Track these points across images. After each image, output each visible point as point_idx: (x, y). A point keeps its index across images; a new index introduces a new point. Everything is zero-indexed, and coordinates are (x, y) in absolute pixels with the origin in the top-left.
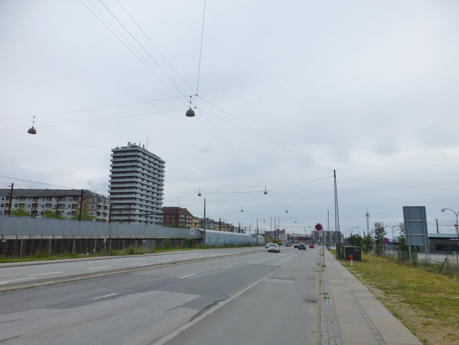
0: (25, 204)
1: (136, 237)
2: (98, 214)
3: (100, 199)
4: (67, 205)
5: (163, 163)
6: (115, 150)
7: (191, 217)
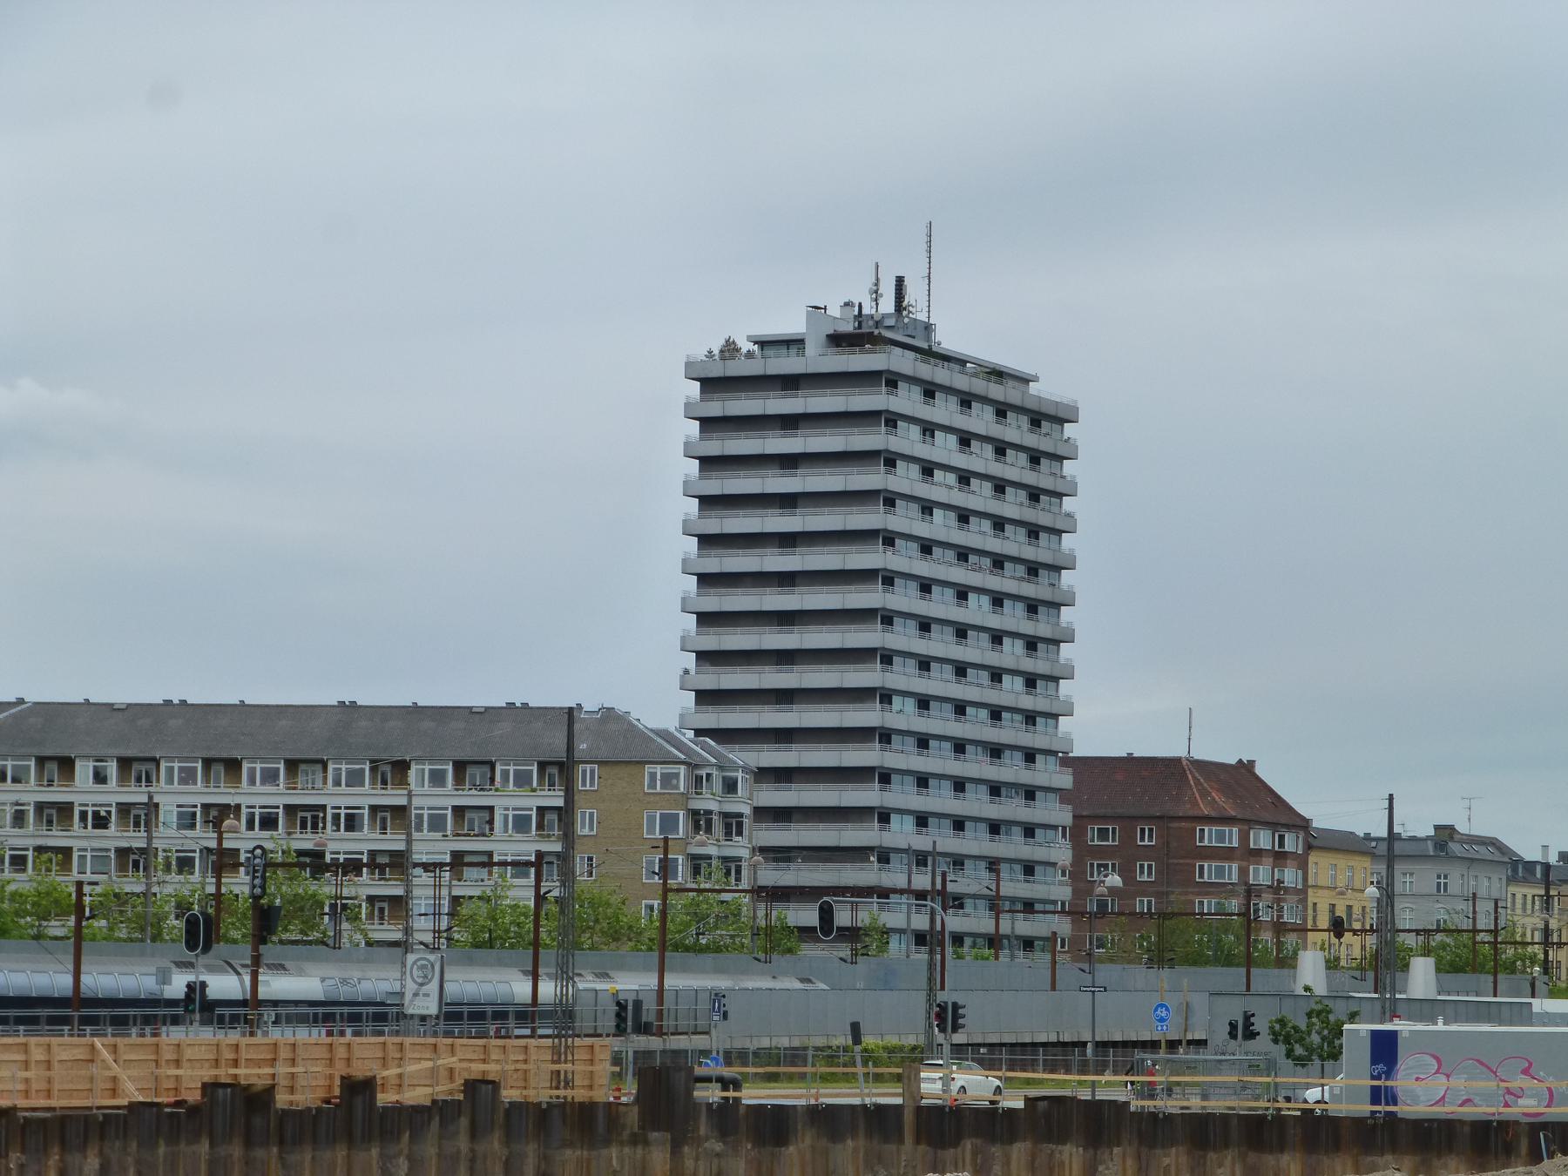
0: (244, 811)
1: (1058, 1037)
2: (1162, 1030)
3: (703, 772)
4: (506, 817)
5: (1060, 419)
6: (716, 371)
7: (1292, 843)
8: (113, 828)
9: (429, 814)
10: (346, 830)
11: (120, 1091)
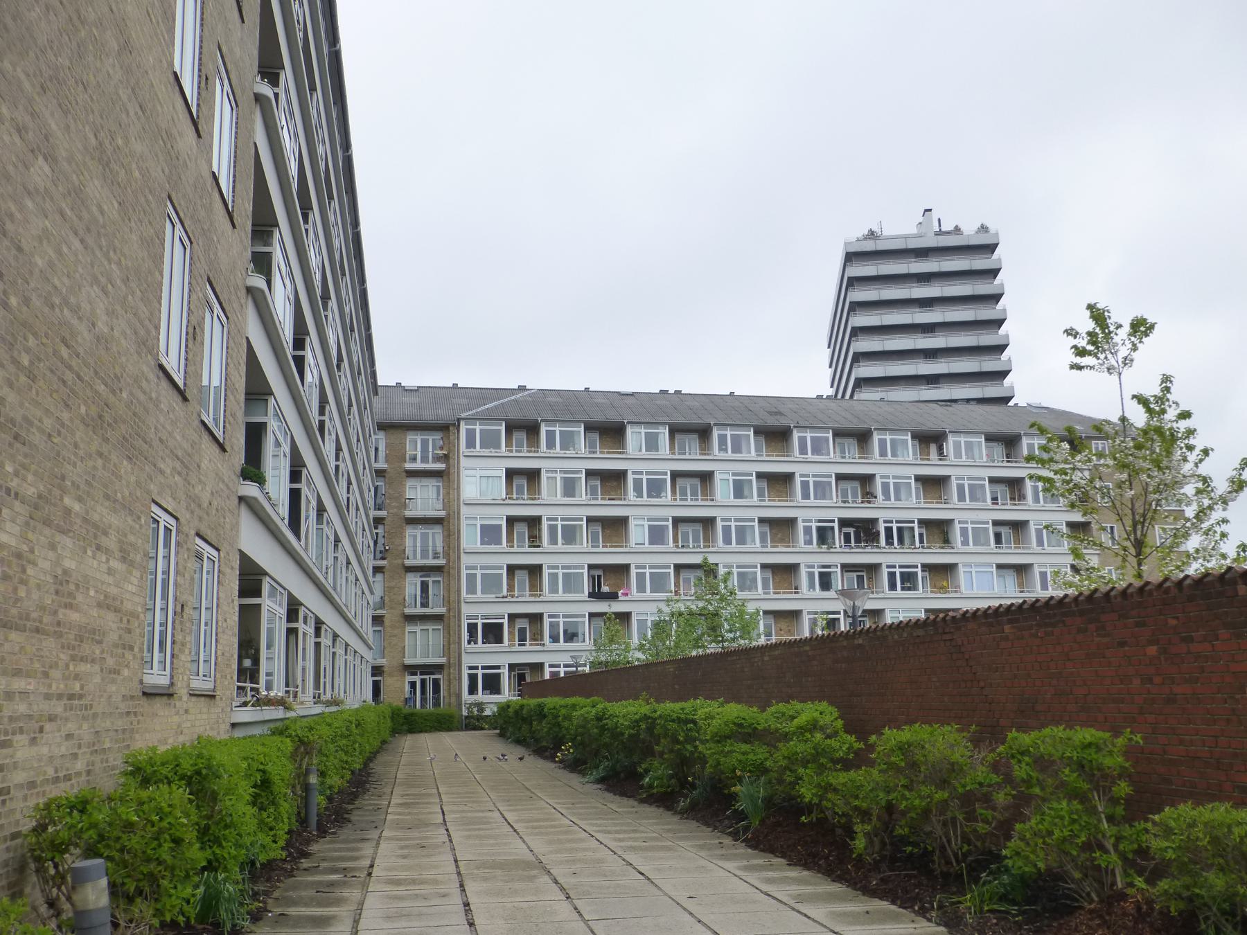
8: (667, 497)
9: (814, 481)
10: (738, 543)
11: (703, 862)
